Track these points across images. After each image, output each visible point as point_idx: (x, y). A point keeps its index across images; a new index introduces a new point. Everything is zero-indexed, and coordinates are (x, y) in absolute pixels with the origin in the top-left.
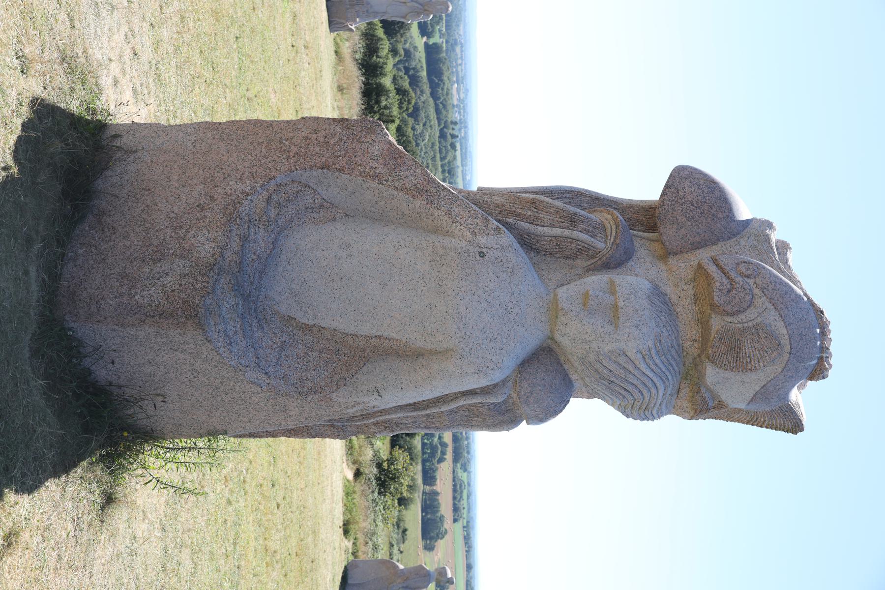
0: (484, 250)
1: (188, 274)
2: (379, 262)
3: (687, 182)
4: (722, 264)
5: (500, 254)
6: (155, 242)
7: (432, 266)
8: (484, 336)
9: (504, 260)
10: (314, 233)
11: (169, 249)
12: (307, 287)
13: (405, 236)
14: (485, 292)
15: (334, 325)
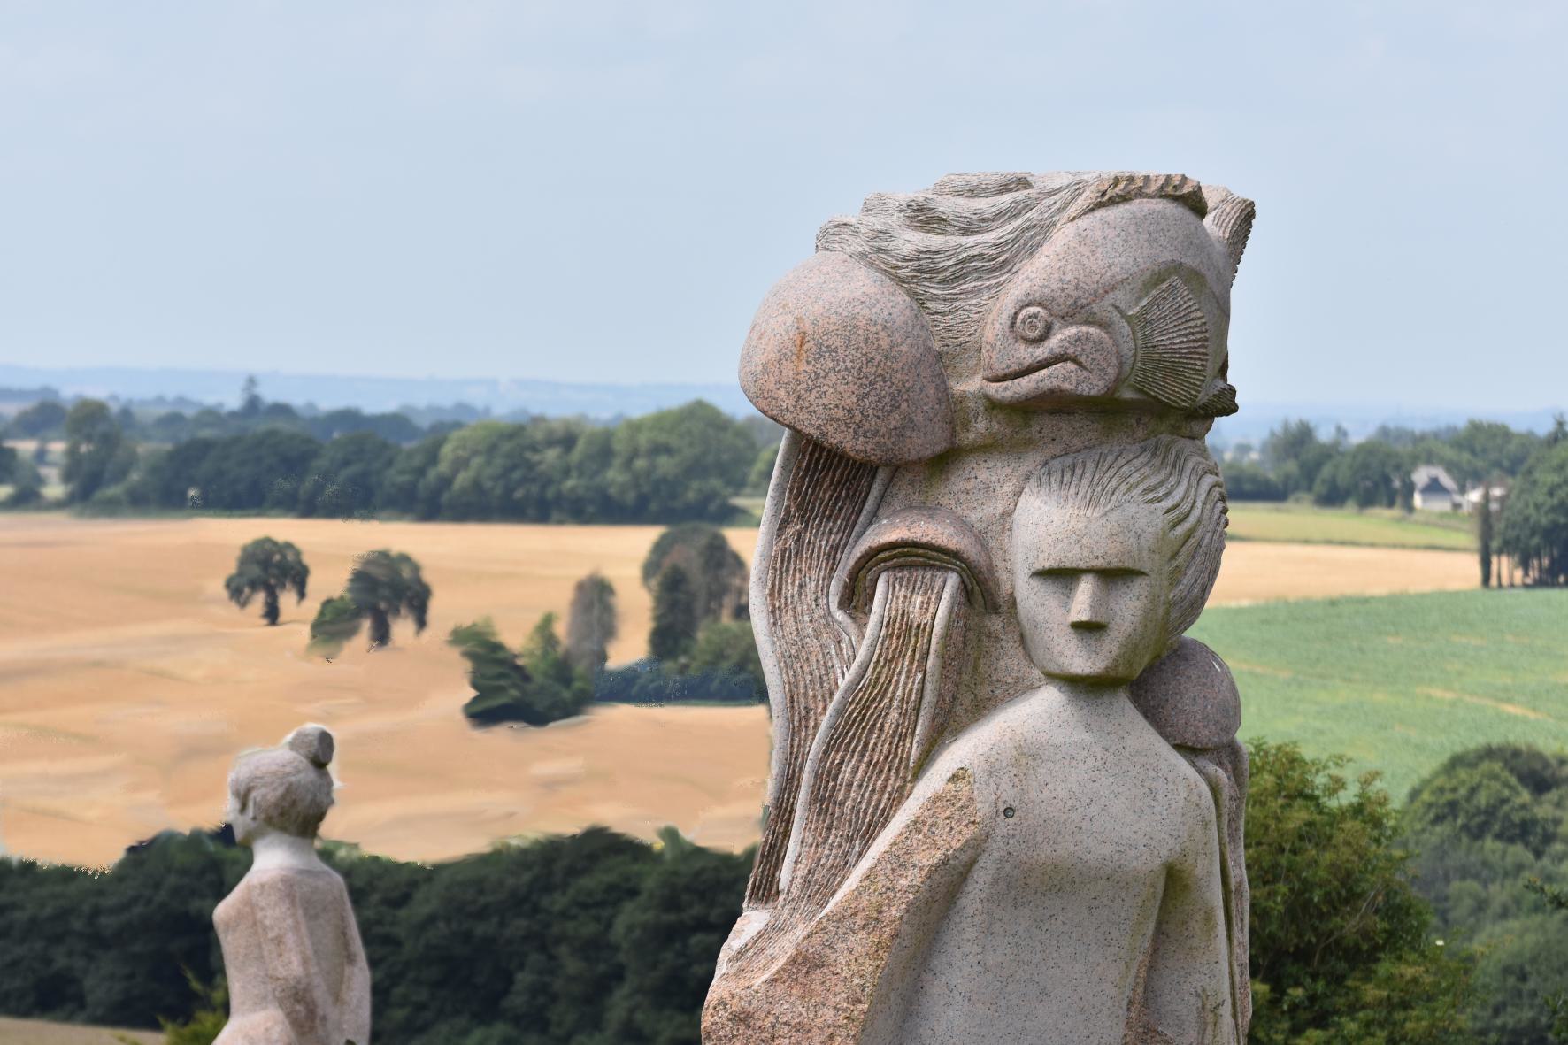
4: (1014, 368)
5: (1006, 779)
8: (1148, 811)
9: (1015, 771)
13: (958, 953)
14: (1074, 808)
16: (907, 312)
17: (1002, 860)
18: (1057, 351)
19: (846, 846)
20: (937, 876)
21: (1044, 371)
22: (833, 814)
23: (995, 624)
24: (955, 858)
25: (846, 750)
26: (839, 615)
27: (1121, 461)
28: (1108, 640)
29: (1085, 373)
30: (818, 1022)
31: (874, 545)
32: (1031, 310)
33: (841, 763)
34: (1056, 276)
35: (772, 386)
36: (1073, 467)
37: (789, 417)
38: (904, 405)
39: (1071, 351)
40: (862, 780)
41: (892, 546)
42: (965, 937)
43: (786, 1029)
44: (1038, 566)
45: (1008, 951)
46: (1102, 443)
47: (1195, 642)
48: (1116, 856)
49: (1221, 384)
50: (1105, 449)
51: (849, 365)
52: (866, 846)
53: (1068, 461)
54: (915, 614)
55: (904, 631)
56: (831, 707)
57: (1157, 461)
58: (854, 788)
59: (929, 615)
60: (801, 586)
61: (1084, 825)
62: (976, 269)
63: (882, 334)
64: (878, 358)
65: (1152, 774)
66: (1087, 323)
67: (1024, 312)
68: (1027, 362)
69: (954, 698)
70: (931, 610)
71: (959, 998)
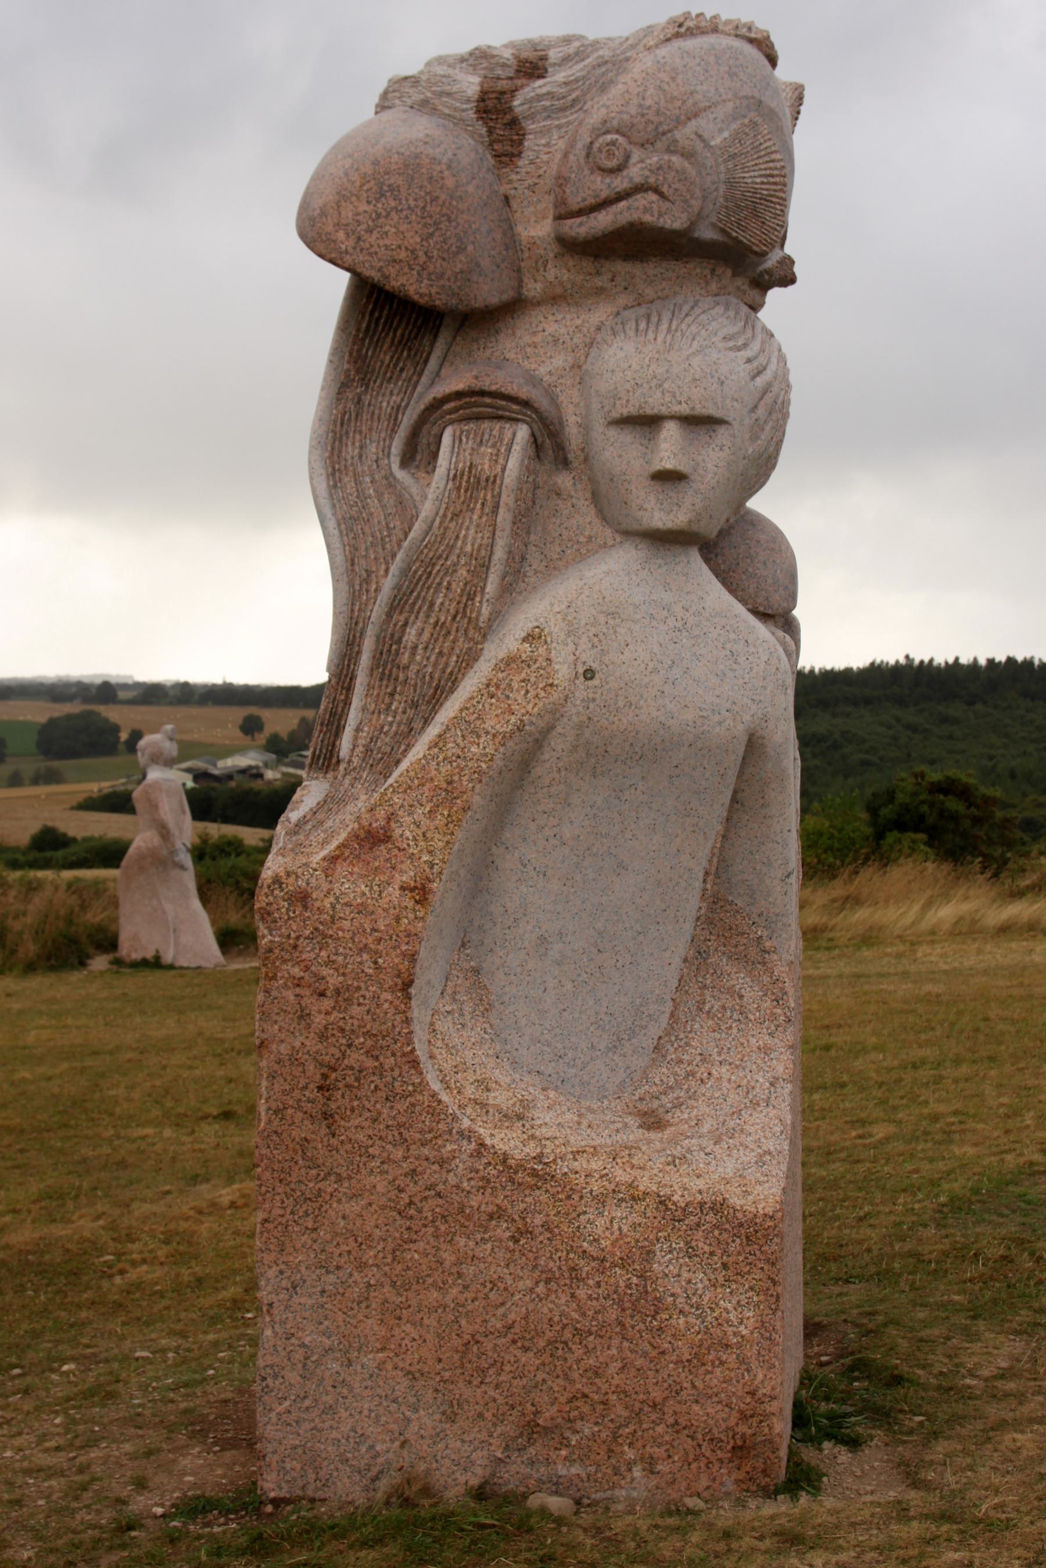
0: (581, 670)
1: (687, 1243)
2: (578, 877)
3: (372, 239)
4: (591, 201)
5: (584, 639)
6: (613, 1314)
7: (602, 774)
8: (730, 674)
9: (593, 630)
10: (511, 1009)
11: (629, 1286)
12: (607, 1018)
13: (533, 826)
14: (656, 671)
15: (677, 961)
16: (473, 155)
17: (580, 726)
18: (638, 180)
19: (410, 713)
20: (510, 744)
21: (623, 204)
22: (396, 679)
23: (564, 480)
24: (532, 723)
25: (411, 611)
26: (400, 474)
27: (697, 311)
28: (690, 492)
29: (668, 204)
30: (384, 903)
31: (439, 395)
32: (609, 137)
33: (406, 624)
34: (635, 101)
35: (330, 228)
36: (648, 317)
37: (348, 259)
38: (470, 248)
39: (652, 180)
40: (428, 643)
41: (459, 395)
42: (540, 808)
43: (348, 910)
44: (615, 415)
45: (586, 823)
46: (675, 294)
47: (758, 516)
48: (699, 722)
49: (781, 254)
50: (679, 299)
51: (412, 203)
52: (434, 711)
53: (642, 310)
54: (485, 467)
55: (471, 485)
56: (394, 569)
57: (732, 313)
58: (420, 651)
59: (499, 468)
60: (361, 447)
61: (667, 688)
62: (545, 109)
63: (446, 173)
64: (443, 197)
65: (732, 636)
66: (669, 151)
67: (601, 140)
68: (604, 195)
69: (523, 558)
70: (501, 461)
71: (533, 873)
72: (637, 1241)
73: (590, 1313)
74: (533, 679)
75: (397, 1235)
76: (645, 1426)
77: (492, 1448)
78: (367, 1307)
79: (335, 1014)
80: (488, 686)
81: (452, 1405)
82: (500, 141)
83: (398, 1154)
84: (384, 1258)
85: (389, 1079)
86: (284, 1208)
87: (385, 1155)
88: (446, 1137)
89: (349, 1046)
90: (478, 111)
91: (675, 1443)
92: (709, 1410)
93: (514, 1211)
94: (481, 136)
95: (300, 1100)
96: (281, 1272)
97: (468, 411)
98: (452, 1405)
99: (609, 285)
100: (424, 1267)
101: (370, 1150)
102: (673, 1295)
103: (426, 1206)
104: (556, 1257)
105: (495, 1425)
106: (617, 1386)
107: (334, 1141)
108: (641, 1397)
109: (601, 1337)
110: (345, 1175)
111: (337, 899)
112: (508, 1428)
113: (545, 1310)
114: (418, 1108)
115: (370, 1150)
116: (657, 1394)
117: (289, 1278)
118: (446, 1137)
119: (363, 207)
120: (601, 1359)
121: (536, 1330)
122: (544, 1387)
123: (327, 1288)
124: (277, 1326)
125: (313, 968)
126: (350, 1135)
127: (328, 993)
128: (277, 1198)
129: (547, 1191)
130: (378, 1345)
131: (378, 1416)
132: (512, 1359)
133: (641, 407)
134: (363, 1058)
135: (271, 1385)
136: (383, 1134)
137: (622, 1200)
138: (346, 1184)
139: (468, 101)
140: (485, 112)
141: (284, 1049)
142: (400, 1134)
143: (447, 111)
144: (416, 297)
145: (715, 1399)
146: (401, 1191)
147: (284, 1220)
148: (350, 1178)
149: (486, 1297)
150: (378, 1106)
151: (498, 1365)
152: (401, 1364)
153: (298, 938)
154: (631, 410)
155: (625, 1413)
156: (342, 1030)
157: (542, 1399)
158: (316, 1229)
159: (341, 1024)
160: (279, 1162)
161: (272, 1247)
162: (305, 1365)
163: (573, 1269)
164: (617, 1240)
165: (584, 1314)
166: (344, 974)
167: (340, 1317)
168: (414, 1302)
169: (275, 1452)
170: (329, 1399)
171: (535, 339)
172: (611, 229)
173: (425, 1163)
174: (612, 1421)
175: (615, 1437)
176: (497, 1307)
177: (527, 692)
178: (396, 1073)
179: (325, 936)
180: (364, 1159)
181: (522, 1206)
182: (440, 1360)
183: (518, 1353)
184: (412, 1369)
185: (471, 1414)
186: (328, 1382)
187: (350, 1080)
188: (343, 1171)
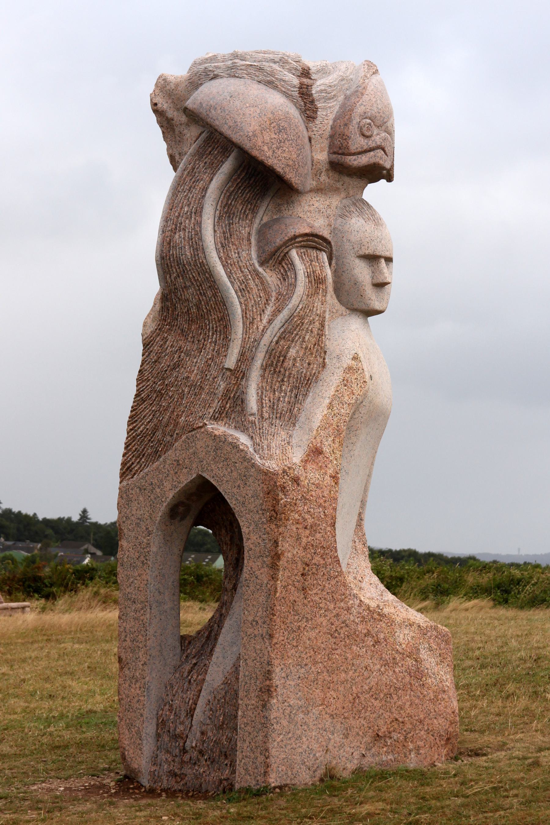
6: (408, 679)
21: (372, 153)
26: (260, 270)
35: (260, 144)
44: (361, 253)
68: (365, 147)
72: (414, 644)
73: (400, 679)
74: (359, 378)
75: (330, 646)
76: (417, 732)
77: (361, 749)
78: (317, 684)
79: (310, 537)
80: (344, 380)
81: (347, 730)
82: (309, 110)
83: (332, 606)
84: (325, 658)
85: (328, 569)
86: (284, 636)
87: (326, 607)
88: (349, 597)
89: (315, 553)
90: (299, 93)
91: (427, 739)
92: (440, 722)
93: (373, 632)
94: (300, 105)
95: (294, 581)
96: (282, 669)
97: (305, 243)
98: (347, 730)
99: (341, 187)
100: (340, 662)
101: (320, 605)
102: (427, 669)
103: (342, 631)
104: (388, 653)
105: (363, 738)
106: (409, 713)
107: (306, 601)
108: (417, 718)
109: (404, 690)
110: (310, 618)
111: (309, 481)
112: (367, 739)
113: (384, 679)
114: (339, 583)
115: (320, 605)
116: (422, 716)
117: (285, 672)
118: (349, 597)
119: (273, 136)
120: (403, 701)
121: (380, 690)
122: (382, 717)
123: (301, 675)
124: (279, 697)
125: (303, 515)
126: (312, 598)
127: (308, 527)
128: (281, 631)
129: (384, 622)
130: (320, 703)
131: (318, 739)
132: (371, 704)
133: (374, 251)
134: (320, 559)
135: (275, 728)
136: (326, 597)
137: (406, 626)
138: (310, 623)
139: (295, 87)
140: (302, 94)
141: (290, 555)
142: (333, 596)
143: (283, 89)
144: (294, 184)
145: (442, 716)
146: (332, 624)
147: (283, 643)
148: (312, 619)
149: (363, 675)
150: (324, 583)
151: (365, 708)
152: (328, 712)
153: (296, 500)
154: (370, 251)
155: (410, 727)
156: (313, 545)
157: (381, 722)
158: (297, 646)
159: (312, 542)
160: (284, 613)
161: (278, 656)
162: (290, 715)
163: (394, 659)
164: (408, 644)
165: (398, 680)
166: (314, 518)
167: (306, 689)
168: (335, 680)
169: (275, 763)
170: (299, 732)
171: (310, 209)
172: (366, 164)
173: (342, 610)
174: (405, 731)
175: (406, 738)
176: (367, 679)
177: (358, 384)
178: (331, 567)
179: (306, 499)
180: (318, 609)
181: (376, 630)
182: (344, 708)
183: (373, 701)
184: (333, 713)
185: (354, 734)
186: (300, 723)
187: (314, 570)
188: (309, 616)
